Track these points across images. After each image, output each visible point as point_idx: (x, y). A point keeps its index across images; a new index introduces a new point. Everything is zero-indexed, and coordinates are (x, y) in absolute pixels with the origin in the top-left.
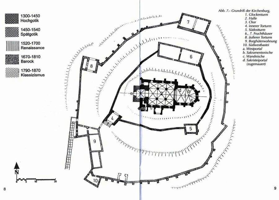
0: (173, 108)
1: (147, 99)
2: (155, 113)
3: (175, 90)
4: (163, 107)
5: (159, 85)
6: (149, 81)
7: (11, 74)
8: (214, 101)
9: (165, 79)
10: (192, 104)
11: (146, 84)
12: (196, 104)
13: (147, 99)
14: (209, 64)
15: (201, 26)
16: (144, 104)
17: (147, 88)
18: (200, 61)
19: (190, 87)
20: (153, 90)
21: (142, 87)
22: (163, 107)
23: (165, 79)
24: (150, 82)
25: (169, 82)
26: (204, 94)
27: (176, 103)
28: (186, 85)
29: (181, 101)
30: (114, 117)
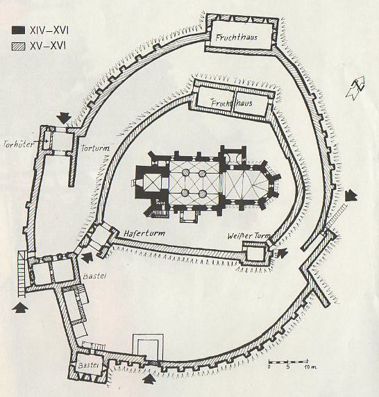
0: (224, 151)
1: (164, 194)
2: (182, 221)
3: (221, 172)
4: (199, 209)
5: (187, 165)
6: (167, 158)
7: (14, 46)
8: (320, 279)
9: (199, 153)
10: (262, 203)
11: (162, 164)
12: (271, 203)
13: (164, 194)
14: (291, 108)
15: (258, 105)
16: (158, 203)
17: (165, 172)
18: (272, 39)
19: (256, 168)
20: (175, 176)
21: (153, 169)
22: (199, 209)
23: (199, 153)
24: (170, 172)
25: (207, 159)
26: (286, 187)
27: (223, 202)
28: (241, 209)
29: (232, 196)
30: (101, 236)
